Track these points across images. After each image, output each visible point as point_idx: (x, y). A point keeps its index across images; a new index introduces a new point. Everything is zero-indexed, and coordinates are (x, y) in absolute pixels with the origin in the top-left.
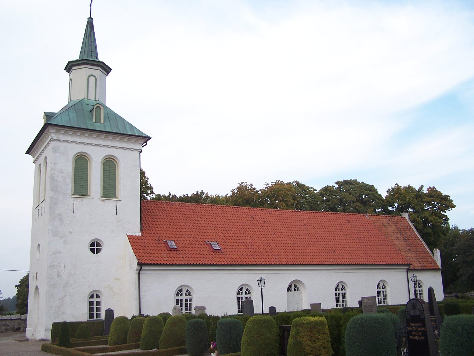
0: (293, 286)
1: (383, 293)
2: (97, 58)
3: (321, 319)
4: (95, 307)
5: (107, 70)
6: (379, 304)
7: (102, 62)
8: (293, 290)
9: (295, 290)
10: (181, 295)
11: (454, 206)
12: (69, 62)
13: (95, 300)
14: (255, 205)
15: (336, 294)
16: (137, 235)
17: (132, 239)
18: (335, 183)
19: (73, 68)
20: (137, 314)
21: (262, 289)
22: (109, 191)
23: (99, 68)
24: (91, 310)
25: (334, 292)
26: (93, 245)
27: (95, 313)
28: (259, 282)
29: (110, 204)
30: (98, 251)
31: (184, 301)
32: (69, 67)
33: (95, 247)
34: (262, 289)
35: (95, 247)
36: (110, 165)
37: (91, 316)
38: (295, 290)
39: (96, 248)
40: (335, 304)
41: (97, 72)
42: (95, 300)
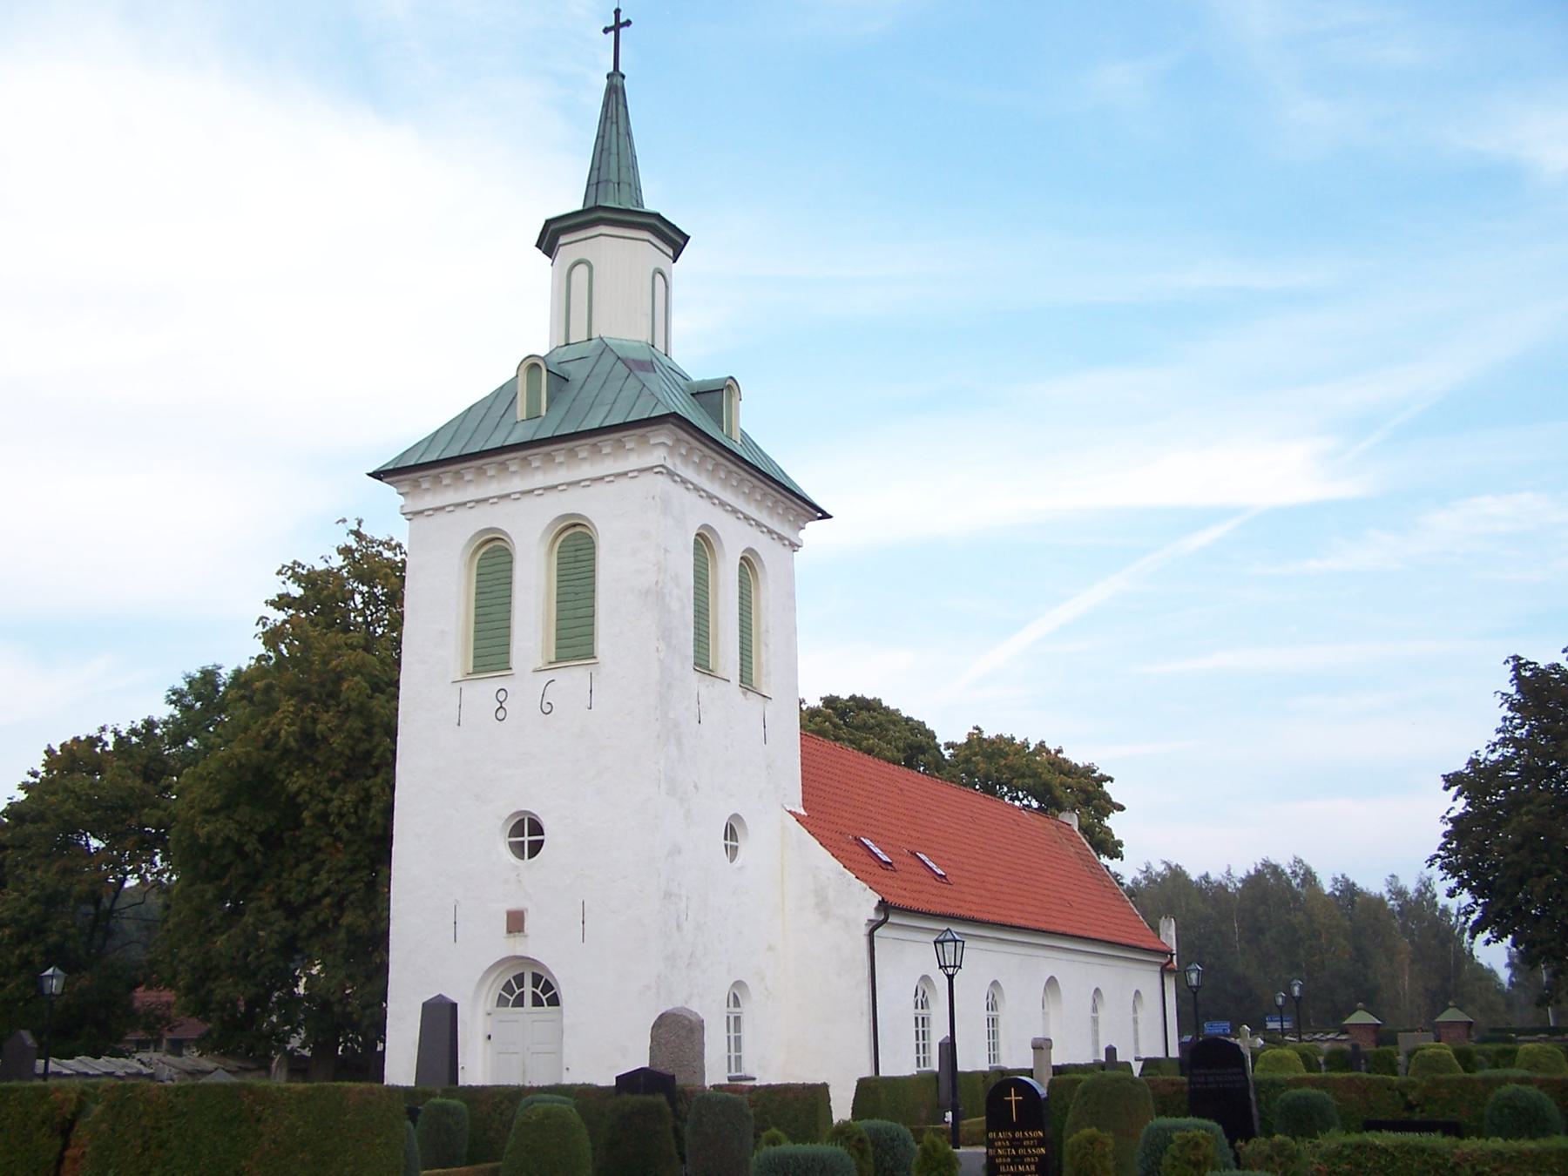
0: (528, 981)
2: (640, 203)
3: (1329, 1097)
5: (675, 241)
7: (658, 216)
8: (528, 999)
9: (537, 1002)
11: (1518, 664)
12: (548, 223)
18: (272, 603)
19: (562, 240)
20: (867, 1072)
21: (951, 978)
23: (646, 235)
32: (551, 237)
33: (528, 835)
34: (951, 978)
35: (528, 835)
36: (576, 548)
38: (537, 1002)
39: (526, 839)
41: (642, 251)
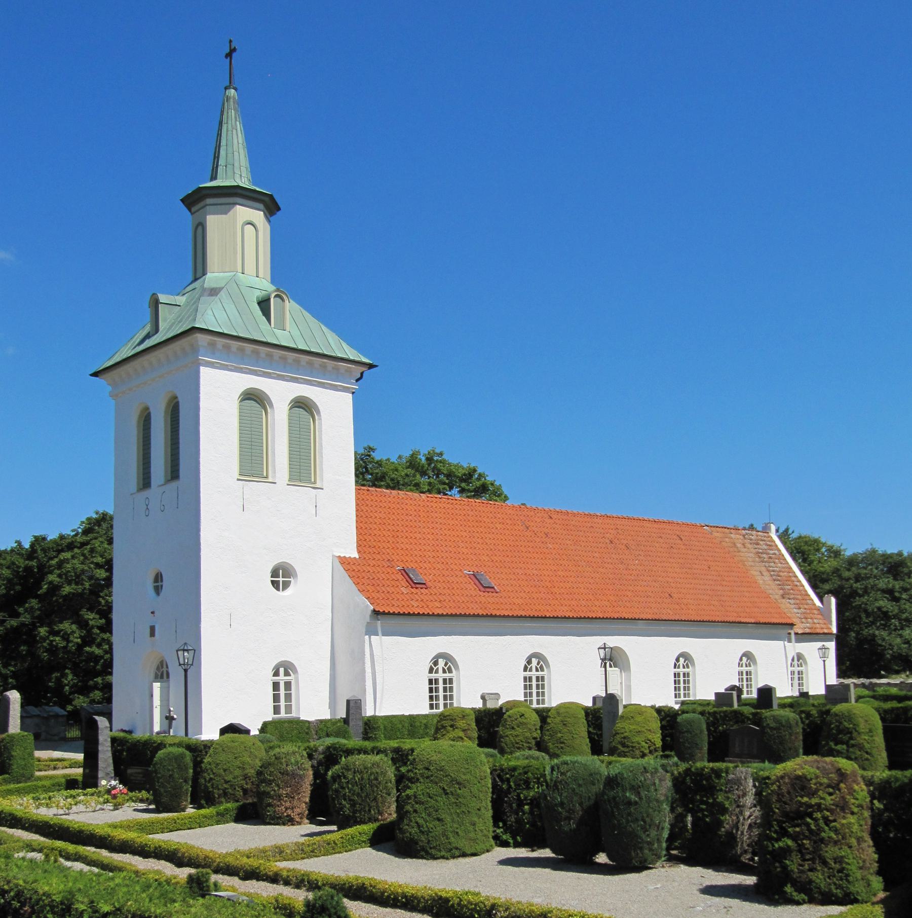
1: (684, 676)
4: (282, 692)
6: (538, 703)
10: (531, 670)
13: (282, 678)
14: (395, 485)
15: (430, 681)
16: (352, 556)
17: (344, 562)
21: (186, 671)
22: (303, 470)
24: (276, 698)
25: (426, 676)
26: (275, 573)
27: (282, 703)
28: (180, 653)
29: (304, 493)
30: (286, 585)
31: (441, 681)
34: (186, 671)
37: (276, 710)
40: (427, 702)
42: (282, 678)
